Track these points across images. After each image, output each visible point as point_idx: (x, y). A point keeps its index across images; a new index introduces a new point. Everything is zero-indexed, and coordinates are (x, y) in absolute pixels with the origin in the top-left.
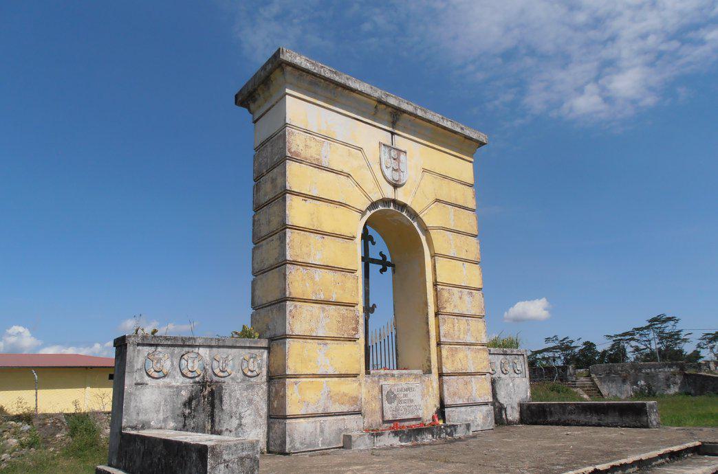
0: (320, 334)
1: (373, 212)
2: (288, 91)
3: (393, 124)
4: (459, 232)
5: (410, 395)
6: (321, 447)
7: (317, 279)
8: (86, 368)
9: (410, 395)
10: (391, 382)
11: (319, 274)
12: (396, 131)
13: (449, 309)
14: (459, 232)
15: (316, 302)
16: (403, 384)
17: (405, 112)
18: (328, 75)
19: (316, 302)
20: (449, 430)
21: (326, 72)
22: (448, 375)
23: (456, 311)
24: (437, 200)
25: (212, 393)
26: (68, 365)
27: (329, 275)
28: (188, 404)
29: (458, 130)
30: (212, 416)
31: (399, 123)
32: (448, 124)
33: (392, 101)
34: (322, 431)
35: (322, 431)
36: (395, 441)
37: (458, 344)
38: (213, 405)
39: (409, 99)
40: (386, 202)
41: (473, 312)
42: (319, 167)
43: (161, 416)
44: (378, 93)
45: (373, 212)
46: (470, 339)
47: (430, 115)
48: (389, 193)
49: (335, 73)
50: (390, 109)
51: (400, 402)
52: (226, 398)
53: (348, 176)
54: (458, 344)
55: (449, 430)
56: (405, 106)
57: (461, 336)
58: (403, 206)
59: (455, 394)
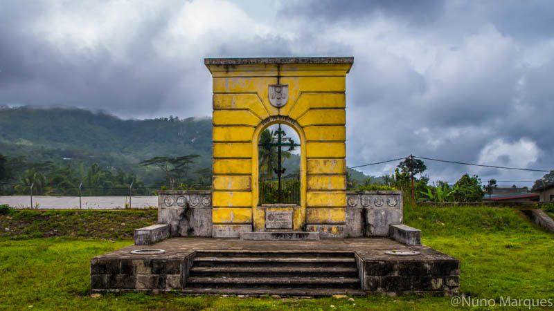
10: (273, 210)
13: (315, 171)
53: (247, 109)
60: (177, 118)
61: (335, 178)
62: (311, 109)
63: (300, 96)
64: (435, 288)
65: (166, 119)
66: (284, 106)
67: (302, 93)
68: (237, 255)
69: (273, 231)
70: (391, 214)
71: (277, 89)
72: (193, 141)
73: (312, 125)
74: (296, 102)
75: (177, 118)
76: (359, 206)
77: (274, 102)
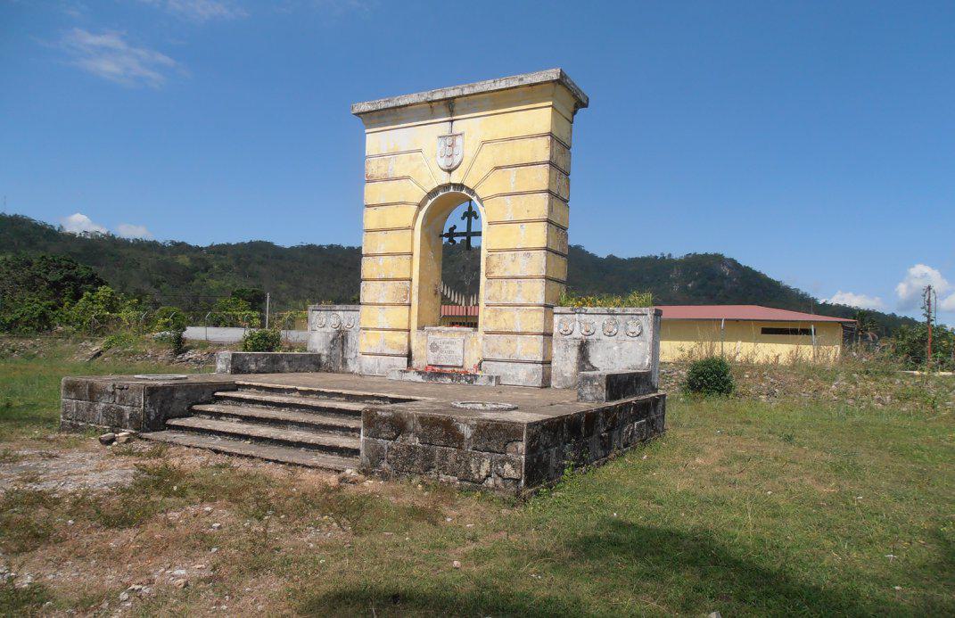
0: (381, 302)
1: (433, 199)
2: (367, 131)
3: (452, 113)
4: (521, 193)
5: (452, 347)
6: (377, 374)
7: (381, 264)
8: (737, 321)
9: (452, 347)
10: (438, 336)
11: (382, 260)
12: (454, 118)
13: (497, 273)
14: (521, 193)
15: (380, 280)
16: (448, 338)
17: (454, 98)
18: (383, 105)
19: (380, 280)
20: (469, 378)
21: (383, 105)
22: (404, 330)
23: (506, 274)
24: (497, 168)
25: (343, 337)
26: (772, 318)
27: (389, 259)
28: (332, 342)
29: (516, 83)
30: (343, 349)
31: (456, 108)
32: (502, 85)
33: (438, 96)
34: (379, 364)
35: (379, 364)
36: (419, 379)
37: (504, 305)
38: (343, 344)
39: (454, 84)
40: (446, 187)
41: (528, 274)
42: (387, 180)
43: (321, 347)
44: (426, 96)
45: (433, 199)
46: (519, 300)
47: (478, 88)
48: (444, 179)
49: (389, 101)
50: (441, 103)
51: (442, 352)
52: (349, 340)
53: (409, 178)
54: (504, 305)
55: (469, 378)
56: (452, 93)
57: (509, 298)
58: (461, 186)
59: (494, 350)
60: (670, 255)
61: (527, 284)
62: (497, 168)
63: (480, 150)
64: (477, 477)
65: (656, 257)
66: (456, 167)
67: (484, 142)
68: (252, 390)
69: (437, 368)
70: (243, 291)
71: (449, 141)
72: (690, 285)
73: (497, 196)
74: (474, 160)
75: (670, 255)
76: (577, 334)
77: (443, 163)
